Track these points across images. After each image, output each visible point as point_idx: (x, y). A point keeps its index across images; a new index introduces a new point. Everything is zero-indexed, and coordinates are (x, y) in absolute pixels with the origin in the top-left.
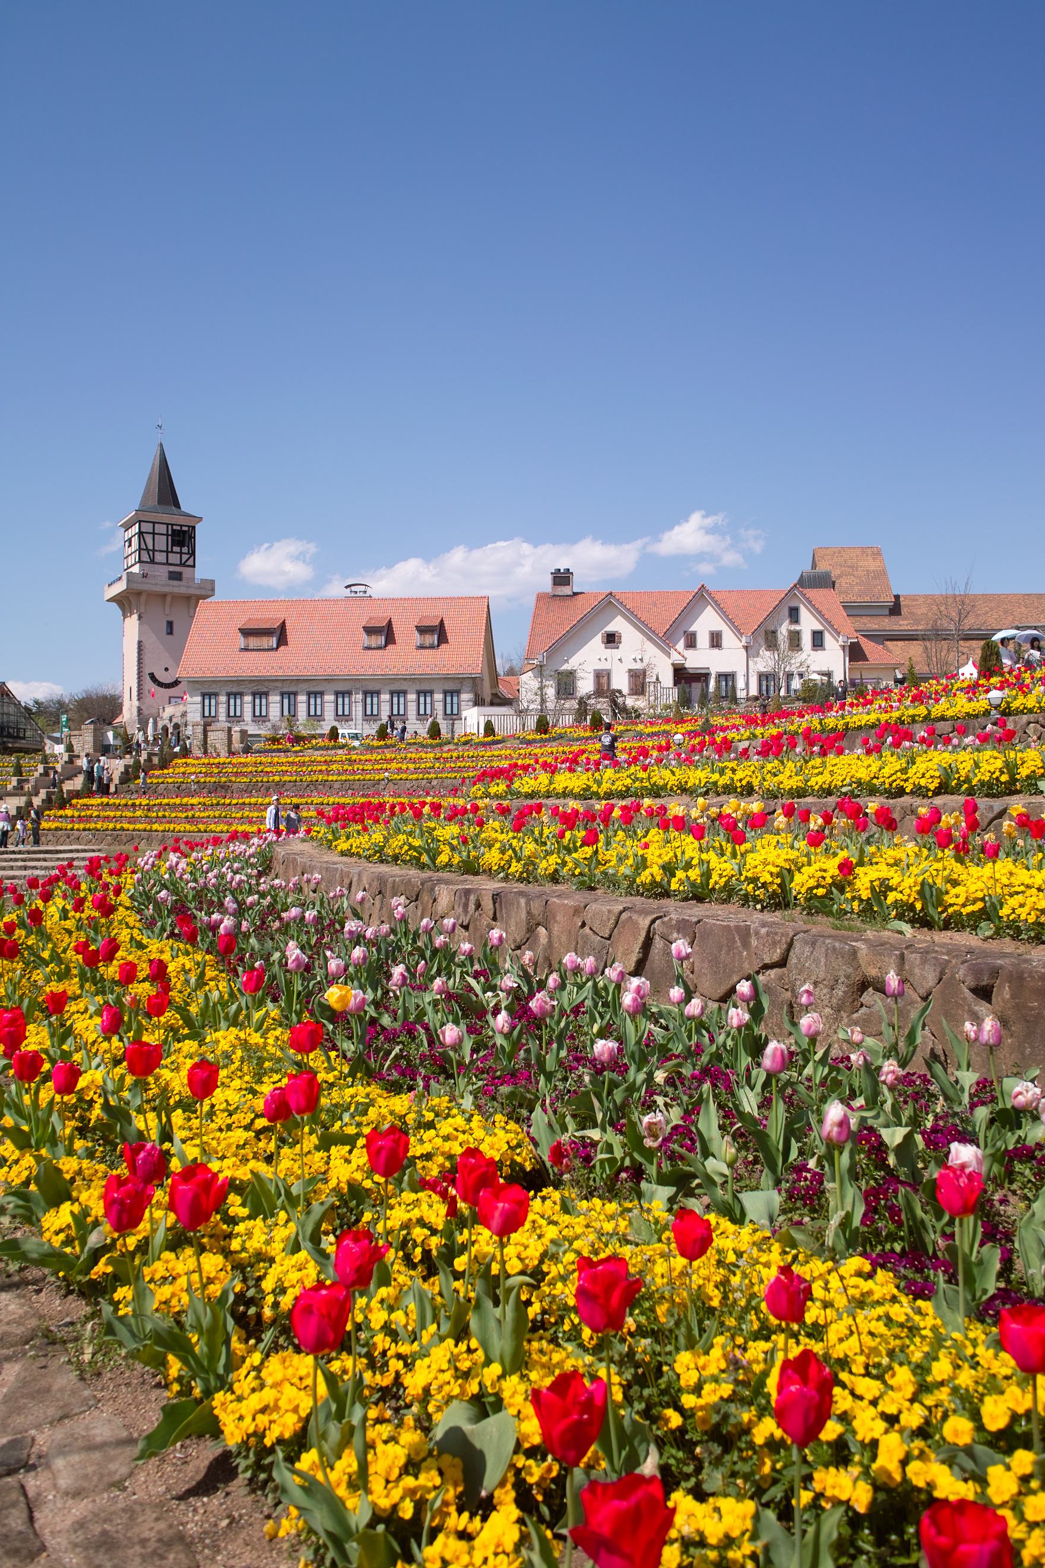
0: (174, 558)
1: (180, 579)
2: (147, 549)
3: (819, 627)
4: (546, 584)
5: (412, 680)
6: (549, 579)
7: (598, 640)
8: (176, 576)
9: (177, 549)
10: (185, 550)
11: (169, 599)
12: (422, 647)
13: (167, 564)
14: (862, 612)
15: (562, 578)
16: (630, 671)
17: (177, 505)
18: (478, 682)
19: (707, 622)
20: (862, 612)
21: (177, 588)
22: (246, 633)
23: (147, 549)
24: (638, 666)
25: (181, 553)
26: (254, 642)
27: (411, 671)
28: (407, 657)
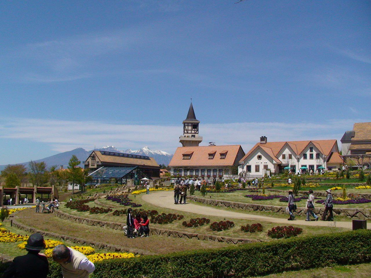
0: (193, 132)
1: (194, 137)
2: (186, 130)
3: (290, 153)
4: (259, 140)
5: (200, 167)
6: (260, 139)
7: (256, 157)
8: (194, 136)
9: (194, 129)
10: (196, 129)
11: (191, 142)
12: (209, 159)
13: (191, 133)
14: (363, 143)
15: (263, 139)
16: (264, 165)
17: (195, 118)
18: (313, 167)
19: (287, 152)
20: (363, 143)
21: (193, 139)
22: (184, 155)
23: (186, 130)
24: (266, 164)
25: (195, 130)
26: (185, 157)
27: (212, 165)
28: (217, 162)
